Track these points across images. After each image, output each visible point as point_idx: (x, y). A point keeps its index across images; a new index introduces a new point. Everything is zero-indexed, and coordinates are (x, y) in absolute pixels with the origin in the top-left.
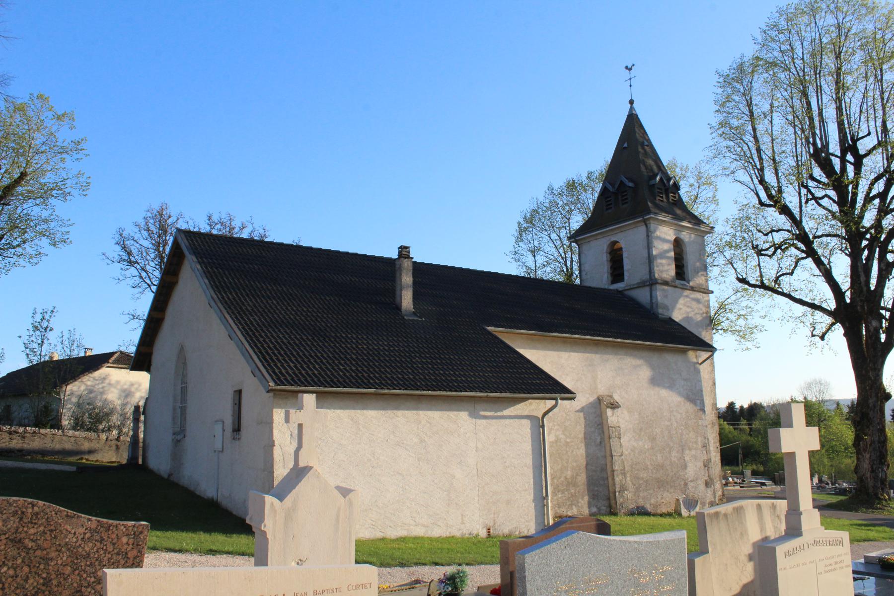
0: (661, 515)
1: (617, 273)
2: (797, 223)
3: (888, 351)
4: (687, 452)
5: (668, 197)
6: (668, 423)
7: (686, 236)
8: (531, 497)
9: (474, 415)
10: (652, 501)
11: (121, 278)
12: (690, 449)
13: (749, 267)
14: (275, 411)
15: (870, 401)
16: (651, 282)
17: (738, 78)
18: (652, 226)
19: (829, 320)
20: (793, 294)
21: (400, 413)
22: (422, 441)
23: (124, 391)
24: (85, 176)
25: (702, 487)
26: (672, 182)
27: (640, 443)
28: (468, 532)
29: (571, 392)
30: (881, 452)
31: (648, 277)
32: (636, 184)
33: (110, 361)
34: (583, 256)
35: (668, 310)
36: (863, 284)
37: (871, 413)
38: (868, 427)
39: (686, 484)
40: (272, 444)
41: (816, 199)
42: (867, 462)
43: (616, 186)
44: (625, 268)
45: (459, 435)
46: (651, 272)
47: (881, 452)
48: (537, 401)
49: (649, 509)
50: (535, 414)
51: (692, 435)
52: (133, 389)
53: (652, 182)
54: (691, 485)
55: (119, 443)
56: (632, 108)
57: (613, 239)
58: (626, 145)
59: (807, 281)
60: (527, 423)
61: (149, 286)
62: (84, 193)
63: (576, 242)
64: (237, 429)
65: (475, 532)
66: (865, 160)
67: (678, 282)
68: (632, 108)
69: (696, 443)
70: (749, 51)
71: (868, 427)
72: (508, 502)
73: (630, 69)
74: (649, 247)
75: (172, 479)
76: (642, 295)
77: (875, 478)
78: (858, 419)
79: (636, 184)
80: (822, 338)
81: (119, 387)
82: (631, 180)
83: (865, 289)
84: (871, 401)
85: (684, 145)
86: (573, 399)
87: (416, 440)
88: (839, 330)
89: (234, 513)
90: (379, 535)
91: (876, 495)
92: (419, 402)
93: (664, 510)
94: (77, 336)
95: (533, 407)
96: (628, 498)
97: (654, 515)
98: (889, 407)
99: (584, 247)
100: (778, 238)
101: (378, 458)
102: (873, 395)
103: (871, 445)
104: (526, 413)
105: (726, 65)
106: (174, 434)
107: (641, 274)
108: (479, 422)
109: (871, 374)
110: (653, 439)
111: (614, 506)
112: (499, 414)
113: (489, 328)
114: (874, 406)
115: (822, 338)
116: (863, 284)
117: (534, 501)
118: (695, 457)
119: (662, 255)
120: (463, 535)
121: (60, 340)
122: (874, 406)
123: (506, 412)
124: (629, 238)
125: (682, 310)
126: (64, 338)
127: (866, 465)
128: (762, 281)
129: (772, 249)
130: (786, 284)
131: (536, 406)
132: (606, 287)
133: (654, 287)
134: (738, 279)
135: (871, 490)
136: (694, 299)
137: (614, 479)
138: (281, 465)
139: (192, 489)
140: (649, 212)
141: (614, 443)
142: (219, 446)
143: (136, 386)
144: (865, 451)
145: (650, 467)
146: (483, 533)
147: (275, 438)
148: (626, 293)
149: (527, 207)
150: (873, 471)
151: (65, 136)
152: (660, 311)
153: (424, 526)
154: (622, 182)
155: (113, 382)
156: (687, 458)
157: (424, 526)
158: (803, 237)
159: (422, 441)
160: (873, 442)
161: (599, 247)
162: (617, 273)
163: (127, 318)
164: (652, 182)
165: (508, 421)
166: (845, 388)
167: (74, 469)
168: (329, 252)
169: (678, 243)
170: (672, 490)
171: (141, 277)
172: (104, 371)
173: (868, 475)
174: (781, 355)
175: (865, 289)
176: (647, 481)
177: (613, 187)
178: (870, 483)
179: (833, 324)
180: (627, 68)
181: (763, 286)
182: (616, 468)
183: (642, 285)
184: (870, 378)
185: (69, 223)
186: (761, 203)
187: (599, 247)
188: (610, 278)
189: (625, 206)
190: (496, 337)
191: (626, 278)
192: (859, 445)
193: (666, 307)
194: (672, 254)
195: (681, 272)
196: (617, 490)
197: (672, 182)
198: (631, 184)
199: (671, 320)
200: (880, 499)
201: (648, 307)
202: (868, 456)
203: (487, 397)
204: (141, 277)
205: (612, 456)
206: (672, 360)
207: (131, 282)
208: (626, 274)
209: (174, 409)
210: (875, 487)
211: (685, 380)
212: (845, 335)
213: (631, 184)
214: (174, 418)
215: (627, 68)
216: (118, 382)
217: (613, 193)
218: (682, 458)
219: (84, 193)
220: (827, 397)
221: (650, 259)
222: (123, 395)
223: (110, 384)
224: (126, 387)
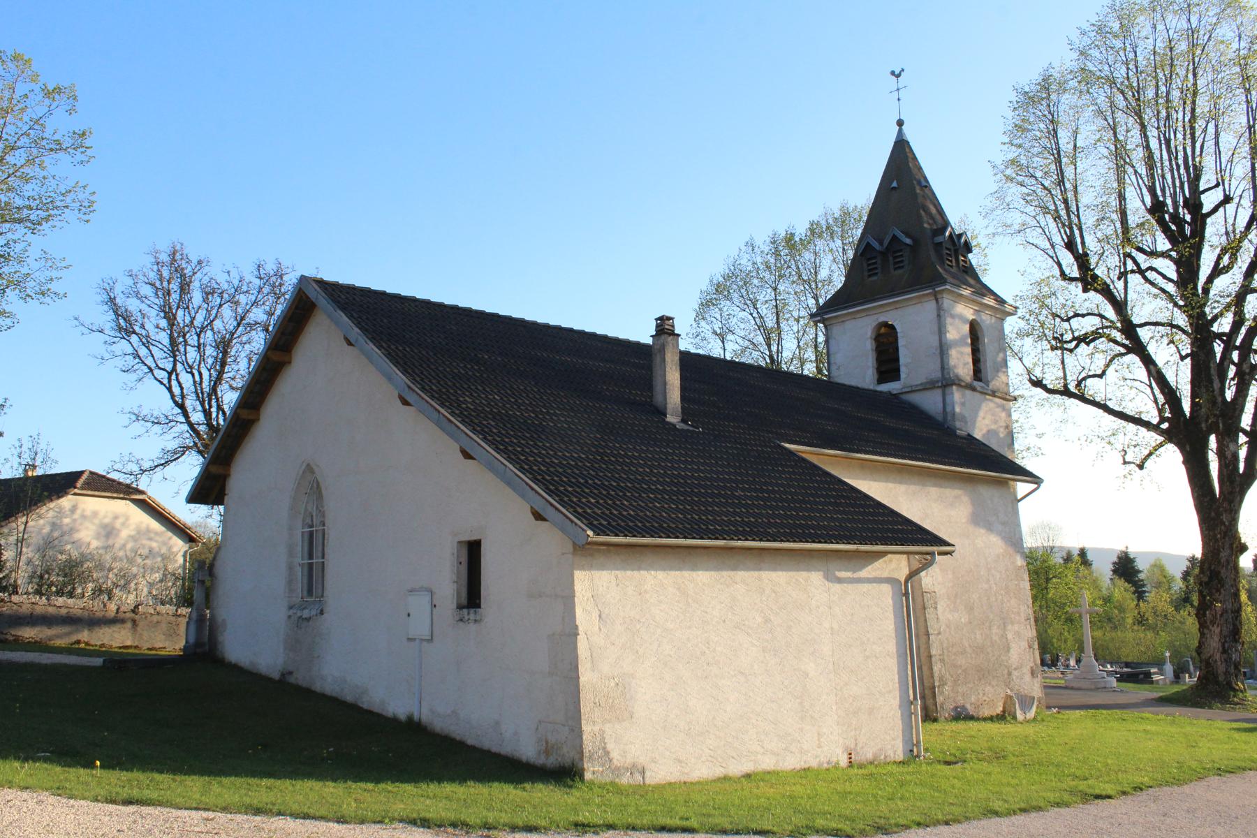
0: (985, 719)
1: (888, 364)
2: (1120, 306)
3: (1249, 485)
4: (1009, 627)
5: (957, 260)
6: (986, 586)
7: (986, 319)
8: (897, 702)
9: (830, 577)
10: (973, 699)
11: (107, 356)
12: (1012, 623)
13: (1051, 368)
14: (579, 575)
15: (1222, 555)
16: (946, 382)
17: (1039, 98)
18: (946, 302)
19: (1154, 438)
20: (1109, 403)
21: (741, 575)
22: (767, 621)
23: (105, 526)
24: (88, 190)
25: (1028, 677)
26: (963, 240)
27: (956, 615)
28: (826, 760)
29: (949, 544)
30: (1234, 625)
31: (939, 375)
32: (906, 244)
33: (79, 485)
34: (832, 342)
35: (966, 422)
36: (1217, 392)
37: (1223, 571)
38: (1218, 590)
39: (1010, 674)
40: (574, 633)
41: (1141, 272)
42: (1217, 639)
43: (886, 242)
44: (902, 361)
45: (810, 610)
46: (943, 367)
47: (1234, 625)
48: (898, 556)
49: (971, 710)
50: (896, 576)
51: (1013, 601)
52: (118, 524)
53: (939, 239)
54: (1015, 673)
55: (137, 617)
56: (900, 132)
57: (882, 319)
58: (895, 184)
59: (1129, 386)
60: (886, 589)
61: (151, 370)
62: (86, 217)
63: (823, 321)
64: (472, 597)
65: (834, 759)
66: (1209, 220)
67: (976, 384)
68: (900, 132)
69: (1019, 613)
70: (1063, 59)
71: (1218, 590)
72: (871, 711)
73: (898, 76)
74: (941, 331)
75: (292, 680)
76: (930, 402)
77: (1228, 661)
78: (1205, 579)
79: (906, 244)
80: (1141, 467)
81: (96, 521)
82: (907, 235)
83: (1220, 399)
84: (1224, 555)
85: (965, 193)
86: (950, 553)
87: (760, 620)
88: (1172, 456)
89: (470, 742)
90: (719, 772)
91: (1229, 684)
92: (761, 558)
93: (987, 712)
94: (43, 446)
95: (893, 565)
96: (947, 698)
97: (978, 719)
98: (1245, 562)
99: (836, 330)
100: (1087, 325)
101: (714, 651)
102: (1227, 546)
103: (1221, 615)
104: (885, 575)
105: (1029, 78)
106: (291, 608)
107: (930, 370)
108: (837, 587)
109: (1224, 517)
110: (970, 609)
111: (932, 707)
112: (857, 575)
113: (787, 445)
114: (1228, 562)
115: (1141, 467)
116: (1217, 392)
117: (900, 707)
118: (1018, 634)
119: (956, 343)
120: (820, 764)
121: (16, 452)
122: (1228, 562)
123: (866, 572)
124: (911, 318)
125: (982, 423)
126: (25, 448)
127: (1214, 643)
128: (1065, 386)
129: (1074, 343)
130: (1094, 388)
131: (896, 564)
132: (871, 387)
133: (948, 390)
134: (1031, 380)
135: (1221, 678)
136: (999, 406)
137: (931, 669)
138: (589, 665)
139: (349, 698)
140: (944, 282)
141: (930, 614)
142: (420, 627)
143: (121, 520)
144: (1213, 623)
145: (969, 650)
146: (844, 762)
147: (578, 622)
148: (904, 397)
149: (718, 270)
150: (1224, 651)
151: (60, 125)
152: (958, 424)
153: (773, 753)
154: (894, 237)
155: (88, 513)
156: (1010, 636)
157: (773, 753)
158: (1129, 329)
159: (767, 621)
160: (1224, 611)
161: (858, 333)
162: (888, 364)
163: (125, 419)
164: (939, 239)
165: (866, 587)
166: (1174, 536)
167: (98, 661)
168: (509, 319)
169: (974, 328)
170: (994, 683)
171: (136, 355)
172: (66, 502)
173: (1217, 656)
174: (1104, 488)
175: (1220, 399)
176: (965, 671)
177: (881, 243)
178: (1221, 668)
179: (186, 448)
180: (893, 73)
181: (1066, 392)
182: (933, 652)
183: (930, 386)
184: (1223, 523)
185: (63, 264)
186: (1063, 275)
187: (858, 333)
188: (876, 377)
189: (900, 271)
190: (804, 460)
191: (903, 376)
192: (1204, 615)
193: (963, 419)
194: (969, 341)
195: (978, 373)
196: (937, 684)
197: (963, 240)
198: (908, 241)
199: (970, 438)
200: (1235, 690)
201: (940, 418)
202: (1217, 630)
203: (857, 551)
204: (136, 355)
205: (928, 635)
206: (987, 492)
207: (120, 362)
208: (903, 369)
209: (291, 568)
210: (1227, 673)
211: (1004, 524)
212: (1184, 462)
213: (908, 241)
214: (290, 582)
215: (893, 73)
216: (95, 514)
217: (881, 253)
218: (1004, 636)
219: (86, 217)
220: (1057, 544)
221: (943, 349)
222: (103, 533)
223: (84, 517)
224: (107, 521)
